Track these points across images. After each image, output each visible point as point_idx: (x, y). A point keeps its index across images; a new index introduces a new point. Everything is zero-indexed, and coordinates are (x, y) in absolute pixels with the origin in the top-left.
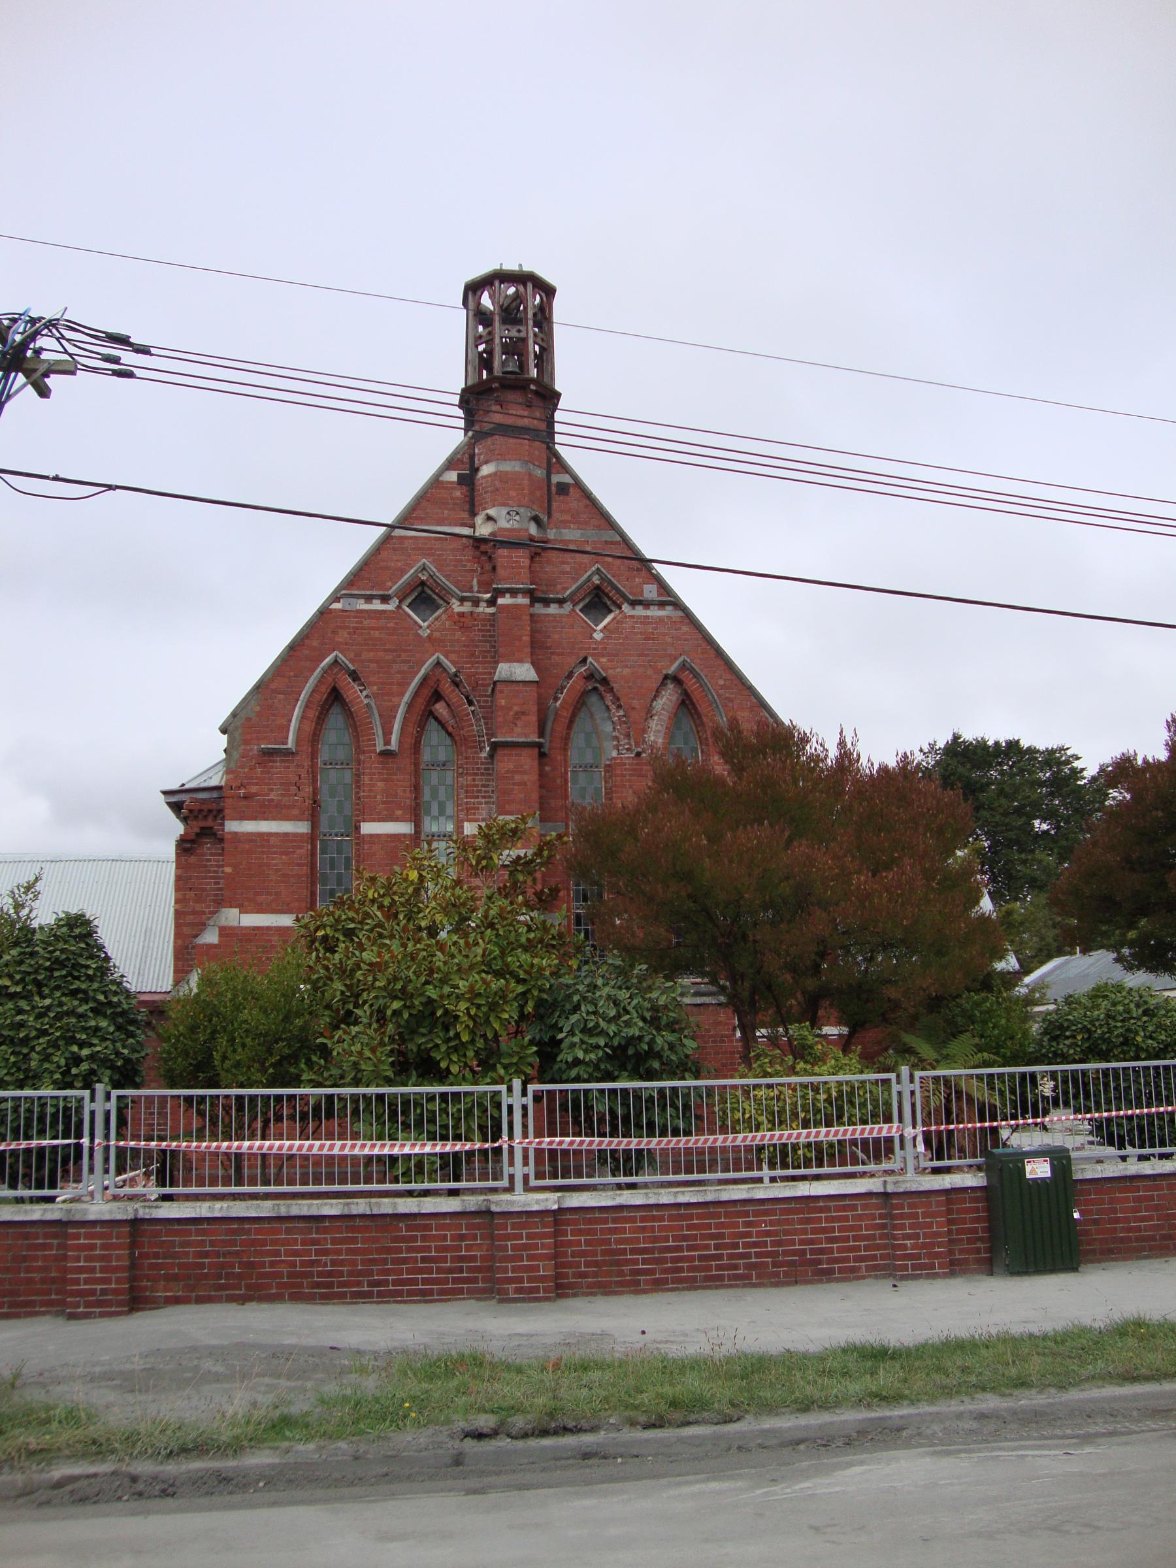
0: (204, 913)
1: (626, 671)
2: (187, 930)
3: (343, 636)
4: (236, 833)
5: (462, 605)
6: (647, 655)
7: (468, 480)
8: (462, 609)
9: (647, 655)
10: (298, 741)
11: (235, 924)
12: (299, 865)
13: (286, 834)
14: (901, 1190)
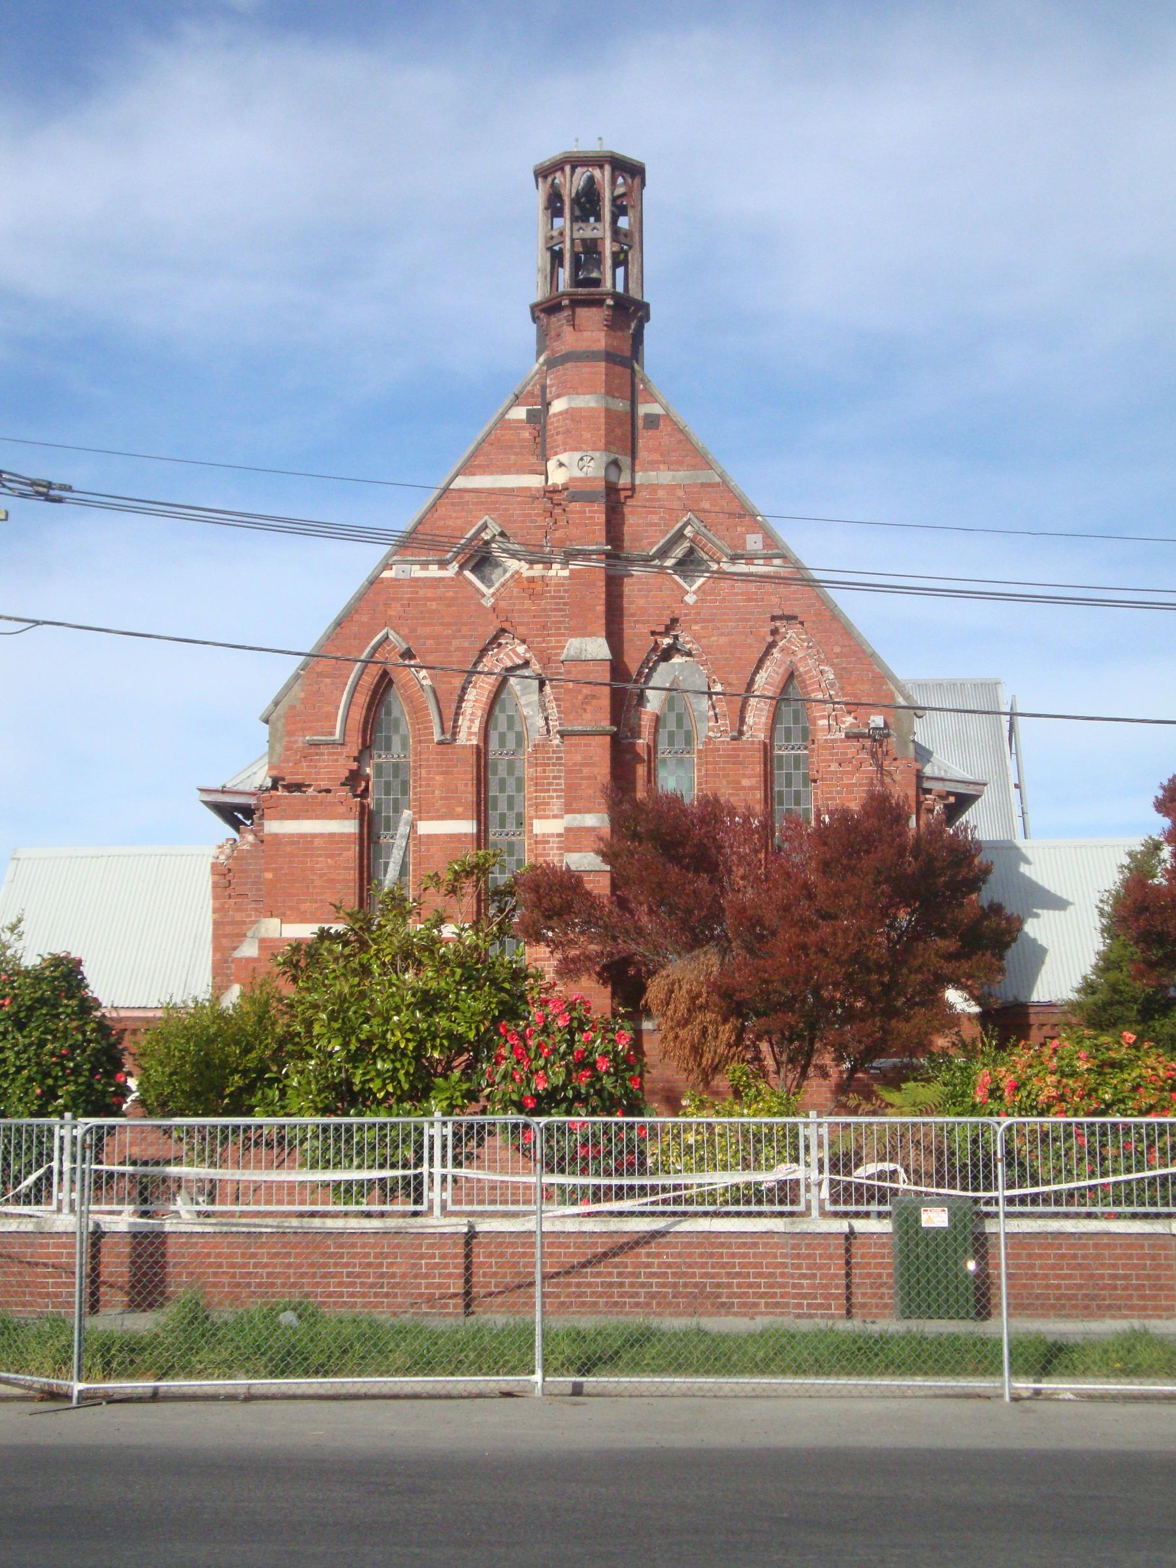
0: (244, 923)
1: (723, 640)
2: (225, 942)
3: (395, 610)
4: (276, 835)
5: (531, 568)
6: (748, 620)
7: (538, 418)
8: (531, 573)
9: (748, 620)
10: (344, 733)
11: (277, 935)
12: (346, 868)
13: (332, 835)
14: (798, 1231)
